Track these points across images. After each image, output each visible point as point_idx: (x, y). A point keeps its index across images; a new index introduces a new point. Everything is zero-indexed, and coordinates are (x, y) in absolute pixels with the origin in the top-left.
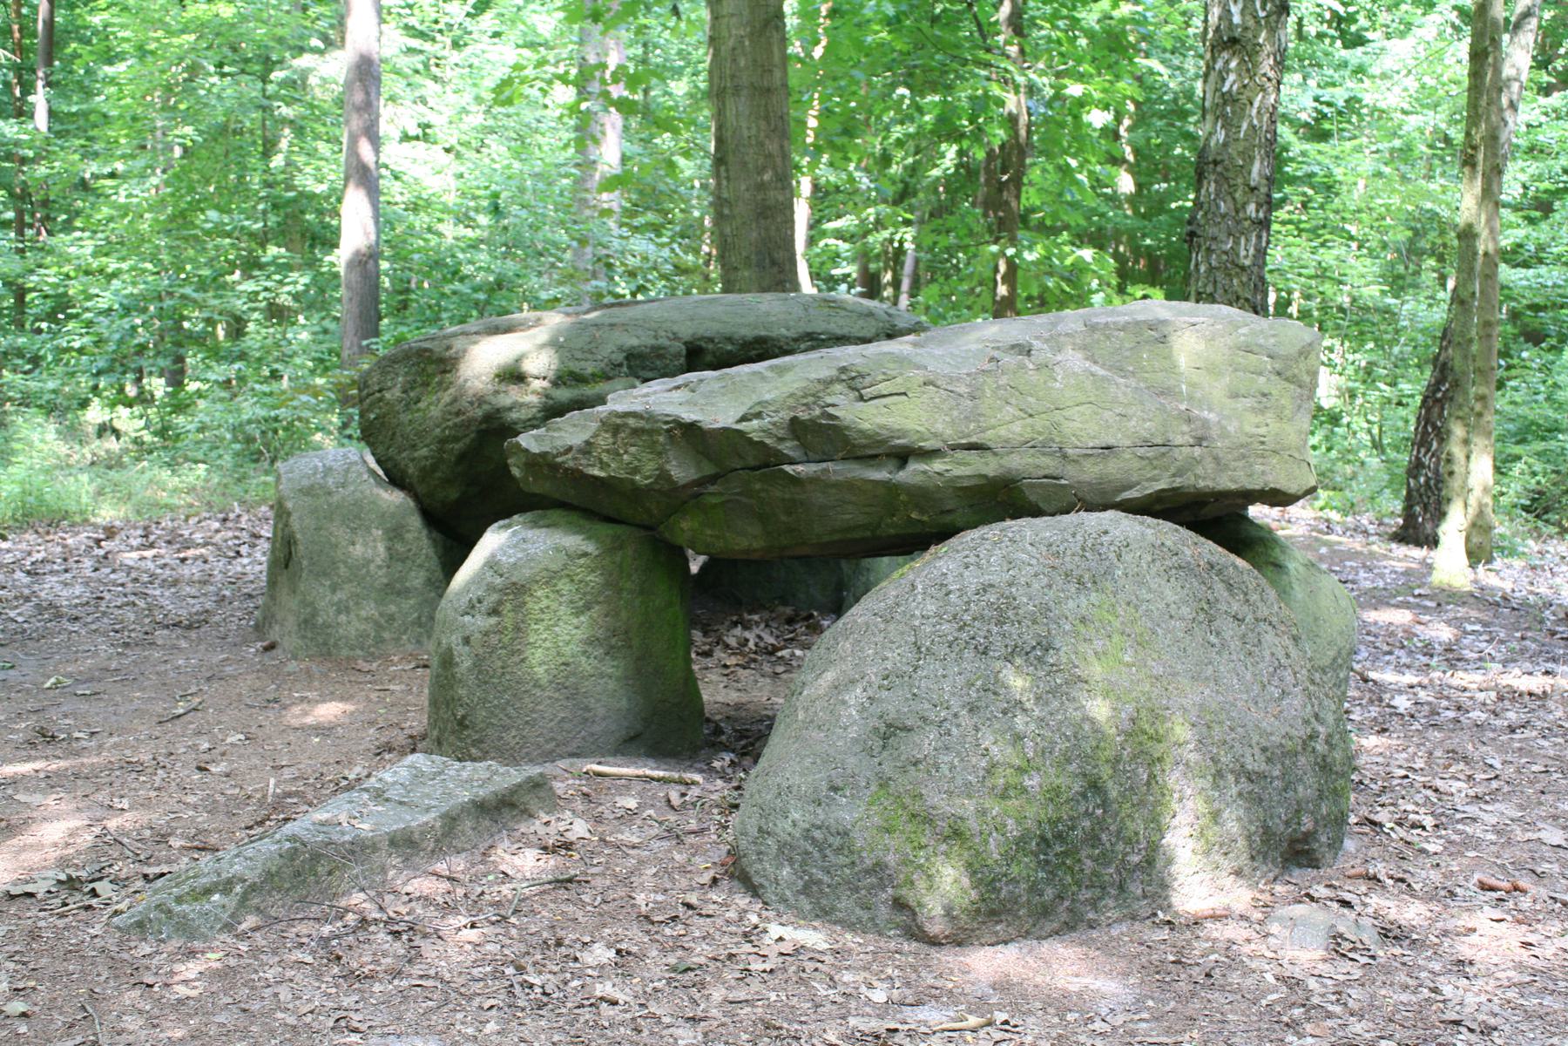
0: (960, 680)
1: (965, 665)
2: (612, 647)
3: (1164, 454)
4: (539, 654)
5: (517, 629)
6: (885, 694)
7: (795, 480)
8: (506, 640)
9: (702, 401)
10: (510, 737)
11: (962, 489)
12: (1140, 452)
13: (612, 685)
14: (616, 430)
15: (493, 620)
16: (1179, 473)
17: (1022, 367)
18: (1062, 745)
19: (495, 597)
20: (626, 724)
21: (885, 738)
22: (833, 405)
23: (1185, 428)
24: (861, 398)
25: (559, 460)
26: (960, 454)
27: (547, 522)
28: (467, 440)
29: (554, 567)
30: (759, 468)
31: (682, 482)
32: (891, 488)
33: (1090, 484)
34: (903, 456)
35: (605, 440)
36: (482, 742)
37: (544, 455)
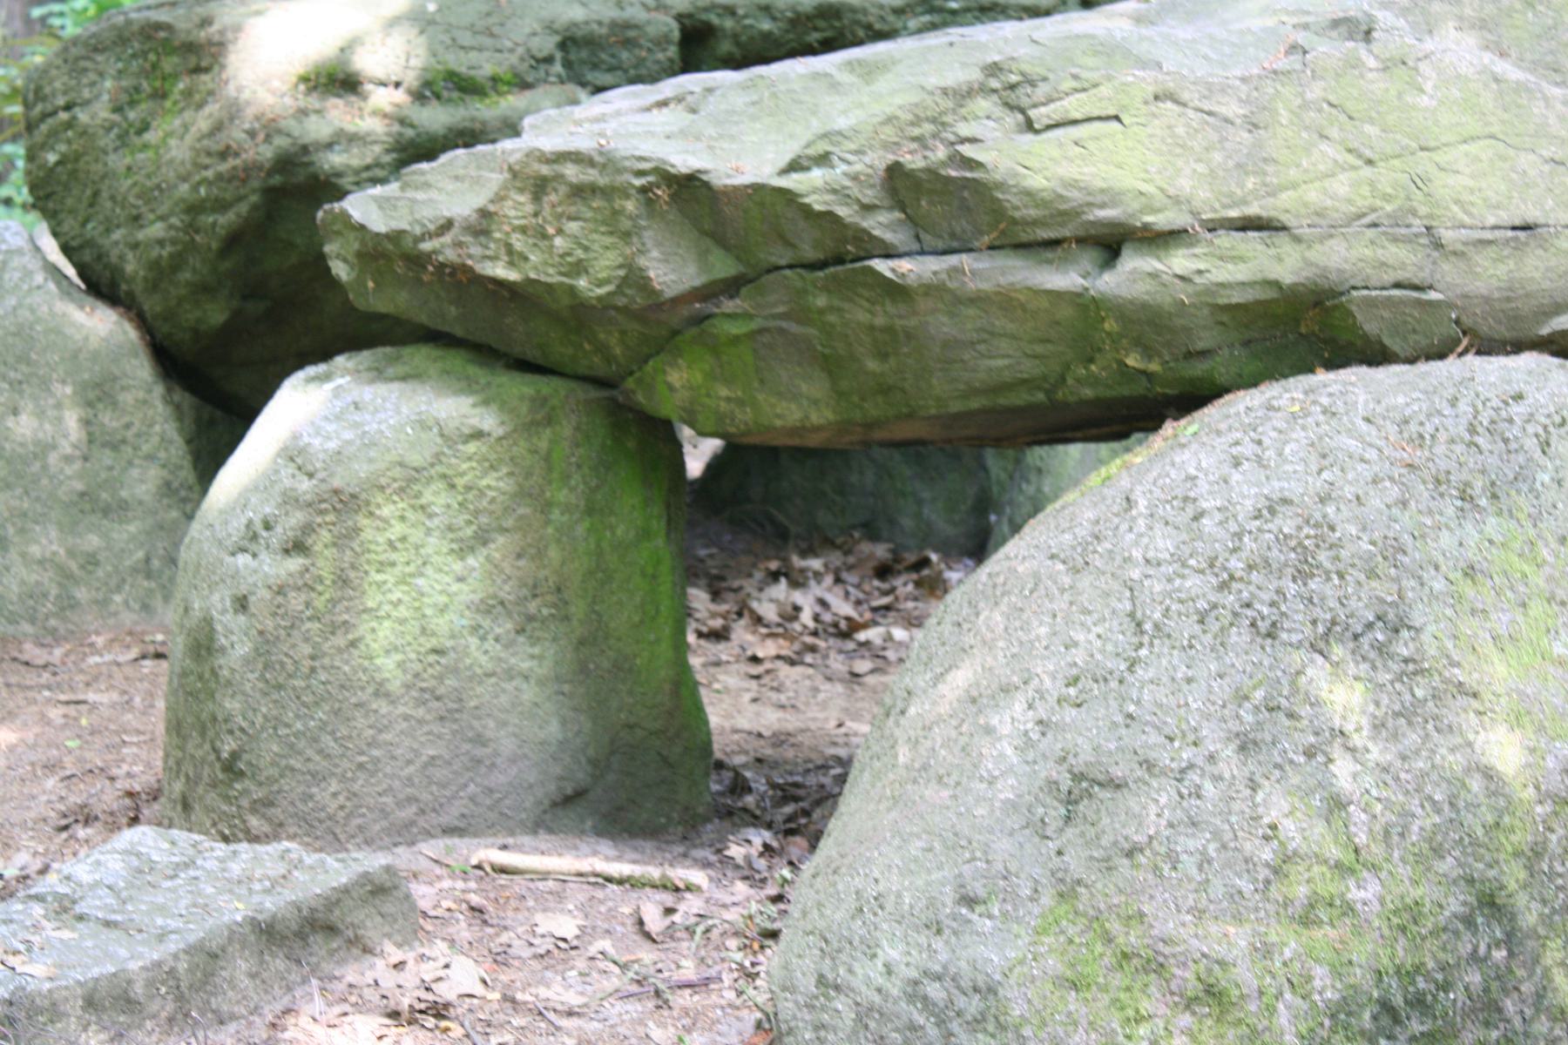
1: (1230, 658)
2: (531, 618)
5: (343, 581)
6: (1070, 713)
7: (895, 290)
8: (320, 603)
9: (711, 131)
13: (529, 693)
14: (540, 187)
15: (295, 563)
17: (1354, 64)
18: (1425, 820)
19: (297, 518)
20: (557, 770)
21: (1071, 800)
22: (973, 140)
25: (426, 246)
26: (1225, 240)
27: (400, 369)
28: (243, 208)
29: (416, 459)
32: (1087, 307)
33: (1487, 300)
35: (517, 208)
36: (271, 804)
37: (396, 236)
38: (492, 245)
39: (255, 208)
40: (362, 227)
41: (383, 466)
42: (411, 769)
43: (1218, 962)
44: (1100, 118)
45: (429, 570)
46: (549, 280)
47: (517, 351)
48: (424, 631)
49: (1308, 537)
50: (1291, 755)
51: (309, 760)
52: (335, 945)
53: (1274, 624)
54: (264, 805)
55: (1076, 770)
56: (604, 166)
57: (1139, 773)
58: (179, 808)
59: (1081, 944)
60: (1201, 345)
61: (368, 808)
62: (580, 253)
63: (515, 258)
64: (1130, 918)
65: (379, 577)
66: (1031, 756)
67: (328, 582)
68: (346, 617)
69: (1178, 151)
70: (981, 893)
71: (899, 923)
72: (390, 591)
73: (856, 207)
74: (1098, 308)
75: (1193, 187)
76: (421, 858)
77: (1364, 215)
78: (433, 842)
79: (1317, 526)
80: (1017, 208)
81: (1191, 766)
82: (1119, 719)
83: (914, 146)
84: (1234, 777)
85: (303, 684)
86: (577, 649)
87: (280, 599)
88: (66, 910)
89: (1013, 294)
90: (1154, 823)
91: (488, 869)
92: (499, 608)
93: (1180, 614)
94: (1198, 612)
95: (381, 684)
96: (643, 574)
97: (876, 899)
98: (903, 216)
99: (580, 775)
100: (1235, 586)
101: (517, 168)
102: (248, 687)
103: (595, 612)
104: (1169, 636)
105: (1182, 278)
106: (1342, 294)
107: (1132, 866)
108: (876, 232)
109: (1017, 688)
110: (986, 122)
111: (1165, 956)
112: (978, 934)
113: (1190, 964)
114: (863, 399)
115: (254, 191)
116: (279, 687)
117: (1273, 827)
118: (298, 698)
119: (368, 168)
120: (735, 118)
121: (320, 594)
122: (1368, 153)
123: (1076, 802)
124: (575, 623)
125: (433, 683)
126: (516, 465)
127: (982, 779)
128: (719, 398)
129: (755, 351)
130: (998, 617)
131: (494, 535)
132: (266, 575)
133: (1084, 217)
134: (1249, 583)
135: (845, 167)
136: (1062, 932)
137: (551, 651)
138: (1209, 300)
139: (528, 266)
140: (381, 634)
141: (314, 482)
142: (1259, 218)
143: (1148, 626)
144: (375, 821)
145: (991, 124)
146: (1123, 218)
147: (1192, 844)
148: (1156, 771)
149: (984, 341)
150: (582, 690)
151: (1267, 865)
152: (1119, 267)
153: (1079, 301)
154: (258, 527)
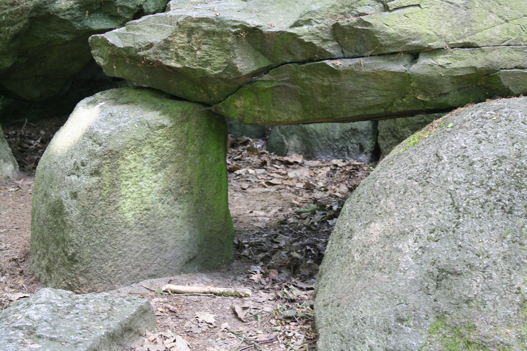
0: (495, 234)
1: (495, 222)
2: (180, 195)
4: (128, 203)
5: (113, 185)
6: (434, 245)
7: (334, 72)
8: (105, 194)
9: (256, 9)
10: (107, 267)
11: (457, 77)
13: (179, 222)
14: (191, 32)
15: (95, 179)
19: (97, 161)
20: (188, 250)
21: (438, 280)
22: (364, 14)
24: (386, 8)
25: (141, 53)
26: (457, 52)
27: (126, 99)
28: (21, 25)
29: (140, 137)
30: (304, 62)
31: (244, 73)
32: (406, 77)
35: (181, 39)
36: (88, 272)
37: (127, 49)
38: (170, 54)
39: (26, 24)
40: (113, 45)
41: (128, 140)
42: (138, 254)
43: (507, 345)
44: (412, 6)
45: (144, 179)
46: (194, 67)
47: (172, 92)
48: (142, 201)
49: (517, 172)
50: (522, 260)
51: (101, 254)
52: (131, 336)
53: (511, 208)
54: (85, 273)
55: (440, 268)
56: (219, 24)
57: (467, 269)
58: (45, 271)
59: (449, 338)
60: (445, 91)
61: (122, 270)
62: (207, 57)
63: (179, 58)
64: (470, 328)
65: (126, 183)
66: (419, 262)
67: (107, 186)
68: (114, 199)
69: (441, 18)
70: (406, 317)
71: (373, 329)
72: (130, 187)
73: (321, 41)
74: (410, 78)
75: (446, 32)
76: (142, 288)
77: (505, 41)
78: (145, 281)
79: (519, 168)
80: (383, 41)
81: (488, 266)
82: (456, 247)
83: (342, 16)
84: (503, 270)
85: (99, 225)
86: (195, 205)
87: (90, 193)
88: (32, 333)
89: (378, 73)
90: (476, 290)
91: (170, 292)
92: (169, 191)
93: (473, 205)
94: (480, 203)
95: (127, 223)
96: (217, 175)
97: (362, 320)
98: (337, 43)
99: (195, 251)
100: (493, 193)
101: (181, 24)
102: (78, 228)
103: (201, 190)
104: (470, 213)
105: (441, 66)
106: (497, 71)
107: (469, 307)
108: (327, 50)
109: (408, 233)
110: (368, 6)
111: (486, 343)
112: (406, 334)
113: (496, 346)
114: (314, 112)
115: (25, 19)
116: (90, 227)
117: (519, 289)
118: (97, 231)
119: (68, 10)
120: (265, 4)
121: (105, 190)
122: (506, 18)
123: (441, 280)
124: (195, 195)
125: (146, 221)
126: (176, 137)
127: (401, 271)
128: (255, 111)
129: (273, 94)
130: (390, 203)
131: (168, 164)
132: (84, 184)
133: (407, 44)
134: (499, 191)
135: (316, 25)
136: (440, 332)
137: (186, 206)
138: (451, 74)
139: (185, 62)
140: (127, 204)
141: (102, 147)
142: (469, 43)
143: (461, 209)
144: (125, 275)
145: (370, 7)
146: (421, 44)
147: (490, 297)
148: (474, 268)
149: (365, 91)
150: (196, 220)
151: (518, 304)
152: (418, 62)
153: (403, 75)
154: (79, 164)
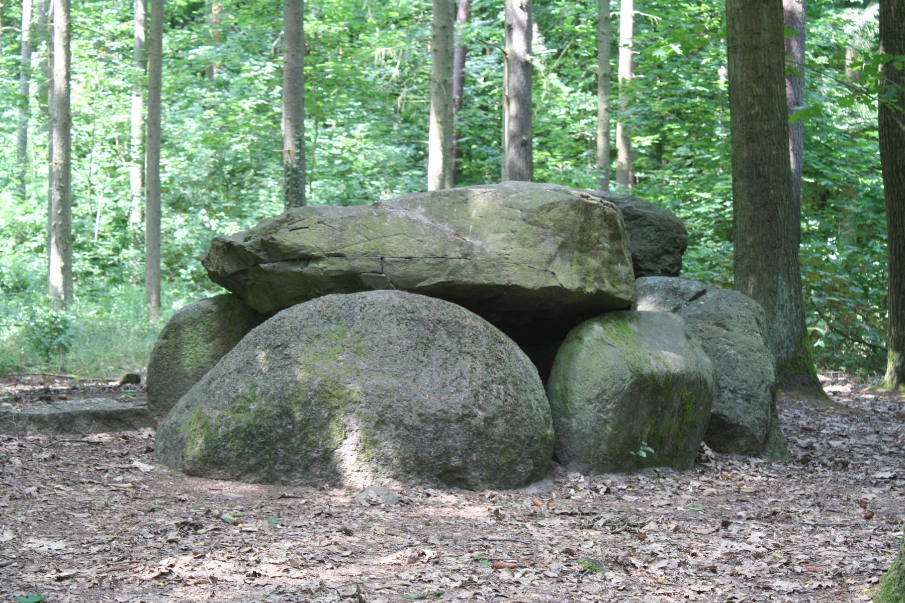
3: (441, 263)
5: (176, 347)
7: (265, 272)
8: (170, 352)
12: (428, 260)
16: (452, 273)
18: (273, 391)
23: (458, 249)
26: (331, 259)
33: (398, 277)
34: (307, 259)
